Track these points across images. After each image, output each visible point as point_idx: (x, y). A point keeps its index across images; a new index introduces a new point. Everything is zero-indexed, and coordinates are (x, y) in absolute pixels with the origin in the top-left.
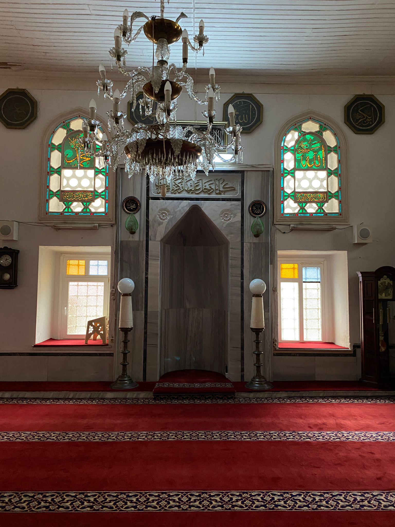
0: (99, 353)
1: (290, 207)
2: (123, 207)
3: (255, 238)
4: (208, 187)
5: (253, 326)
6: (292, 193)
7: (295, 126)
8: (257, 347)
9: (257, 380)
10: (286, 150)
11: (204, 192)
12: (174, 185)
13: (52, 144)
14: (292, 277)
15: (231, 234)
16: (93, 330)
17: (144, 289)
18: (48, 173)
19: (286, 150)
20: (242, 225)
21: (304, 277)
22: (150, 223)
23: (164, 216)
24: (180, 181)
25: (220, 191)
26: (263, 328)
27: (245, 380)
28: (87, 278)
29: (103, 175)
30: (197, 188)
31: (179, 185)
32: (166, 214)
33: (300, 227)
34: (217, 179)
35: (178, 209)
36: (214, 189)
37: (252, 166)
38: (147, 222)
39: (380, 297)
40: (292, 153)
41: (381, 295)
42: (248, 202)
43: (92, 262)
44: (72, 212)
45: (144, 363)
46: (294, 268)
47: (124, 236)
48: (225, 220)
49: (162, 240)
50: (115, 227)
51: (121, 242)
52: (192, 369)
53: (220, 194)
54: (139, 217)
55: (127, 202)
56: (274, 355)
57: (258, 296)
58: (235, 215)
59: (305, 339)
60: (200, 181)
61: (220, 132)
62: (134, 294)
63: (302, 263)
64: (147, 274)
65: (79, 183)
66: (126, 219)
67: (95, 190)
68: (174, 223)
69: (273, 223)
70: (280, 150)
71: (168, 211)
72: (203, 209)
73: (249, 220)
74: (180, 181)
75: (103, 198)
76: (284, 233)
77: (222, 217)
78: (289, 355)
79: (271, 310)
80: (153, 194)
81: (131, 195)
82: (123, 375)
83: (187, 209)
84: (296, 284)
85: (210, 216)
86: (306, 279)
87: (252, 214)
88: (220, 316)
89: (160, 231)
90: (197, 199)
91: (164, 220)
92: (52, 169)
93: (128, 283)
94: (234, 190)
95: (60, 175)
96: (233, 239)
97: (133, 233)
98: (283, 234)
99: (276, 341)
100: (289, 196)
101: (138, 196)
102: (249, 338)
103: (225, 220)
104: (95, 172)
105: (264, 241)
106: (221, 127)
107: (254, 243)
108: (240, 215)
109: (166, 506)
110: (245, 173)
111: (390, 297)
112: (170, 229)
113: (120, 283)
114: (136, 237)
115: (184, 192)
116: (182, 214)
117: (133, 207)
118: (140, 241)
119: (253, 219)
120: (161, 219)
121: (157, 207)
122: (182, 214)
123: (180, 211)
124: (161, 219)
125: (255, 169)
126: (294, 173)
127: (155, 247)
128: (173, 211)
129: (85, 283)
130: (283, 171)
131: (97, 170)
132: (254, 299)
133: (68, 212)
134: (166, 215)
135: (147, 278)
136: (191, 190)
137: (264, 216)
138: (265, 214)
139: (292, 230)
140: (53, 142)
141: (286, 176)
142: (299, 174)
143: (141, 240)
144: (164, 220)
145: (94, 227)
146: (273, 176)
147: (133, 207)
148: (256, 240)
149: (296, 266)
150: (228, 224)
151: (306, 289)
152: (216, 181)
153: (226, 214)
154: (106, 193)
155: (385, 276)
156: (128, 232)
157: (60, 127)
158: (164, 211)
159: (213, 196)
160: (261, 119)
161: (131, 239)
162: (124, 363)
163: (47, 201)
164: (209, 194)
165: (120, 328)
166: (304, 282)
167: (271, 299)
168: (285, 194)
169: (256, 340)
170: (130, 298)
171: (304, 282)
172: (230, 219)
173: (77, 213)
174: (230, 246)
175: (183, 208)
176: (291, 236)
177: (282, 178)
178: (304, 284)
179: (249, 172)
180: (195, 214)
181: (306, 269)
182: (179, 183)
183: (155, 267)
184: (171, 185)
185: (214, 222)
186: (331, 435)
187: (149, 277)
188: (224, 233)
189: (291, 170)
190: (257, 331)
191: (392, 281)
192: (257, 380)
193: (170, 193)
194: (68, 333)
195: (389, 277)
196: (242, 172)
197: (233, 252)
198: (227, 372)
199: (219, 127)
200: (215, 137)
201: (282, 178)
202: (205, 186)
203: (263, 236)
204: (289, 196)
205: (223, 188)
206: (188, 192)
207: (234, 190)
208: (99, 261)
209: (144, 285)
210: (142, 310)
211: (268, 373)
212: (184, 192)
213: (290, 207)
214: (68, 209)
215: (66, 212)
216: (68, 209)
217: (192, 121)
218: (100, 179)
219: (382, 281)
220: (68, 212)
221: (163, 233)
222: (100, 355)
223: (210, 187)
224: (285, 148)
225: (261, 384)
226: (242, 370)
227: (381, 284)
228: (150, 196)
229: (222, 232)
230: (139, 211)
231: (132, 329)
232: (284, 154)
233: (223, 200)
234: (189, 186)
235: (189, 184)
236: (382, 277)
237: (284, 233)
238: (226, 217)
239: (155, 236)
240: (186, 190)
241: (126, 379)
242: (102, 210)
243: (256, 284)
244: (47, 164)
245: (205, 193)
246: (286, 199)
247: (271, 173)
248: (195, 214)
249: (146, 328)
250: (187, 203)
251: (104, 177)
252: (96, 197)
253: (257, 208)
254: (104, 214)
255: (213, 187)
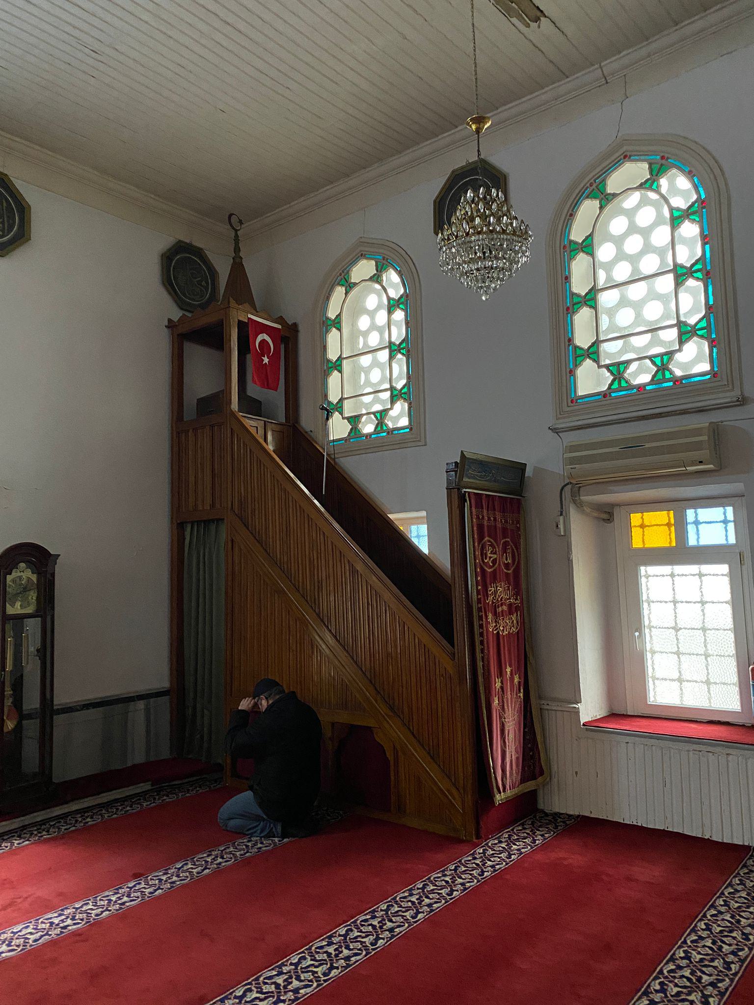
13: (571, 242)
18: (568, 309)
28: (681, 553)
39: (10, 610)
41: (13, 605)
43: (690, 514)
44: (630, 387)
65: (638, 315)
75: (702, 337)
92: (576, 300)
95: (595, 308)
111: (30, 610)
133: (620, 389)
140: (572, 238)
155: (22, 565)
157: (587, 197)
163: (572, 372)
173: (641, 388)
181: (668, 525)
186: (23, 933)
191: (35, 575)
195: (29, 563)
208: (699, 511)
214: (620, 383)
215: (615, 391)
216: (620, 383)
218: (692, 292)
219: (15, 574)
220: (620, 389)
227: (13, 581)
236: (16, 566)
242: (705, 367)
244: (564, 291)
251: (700, 284)
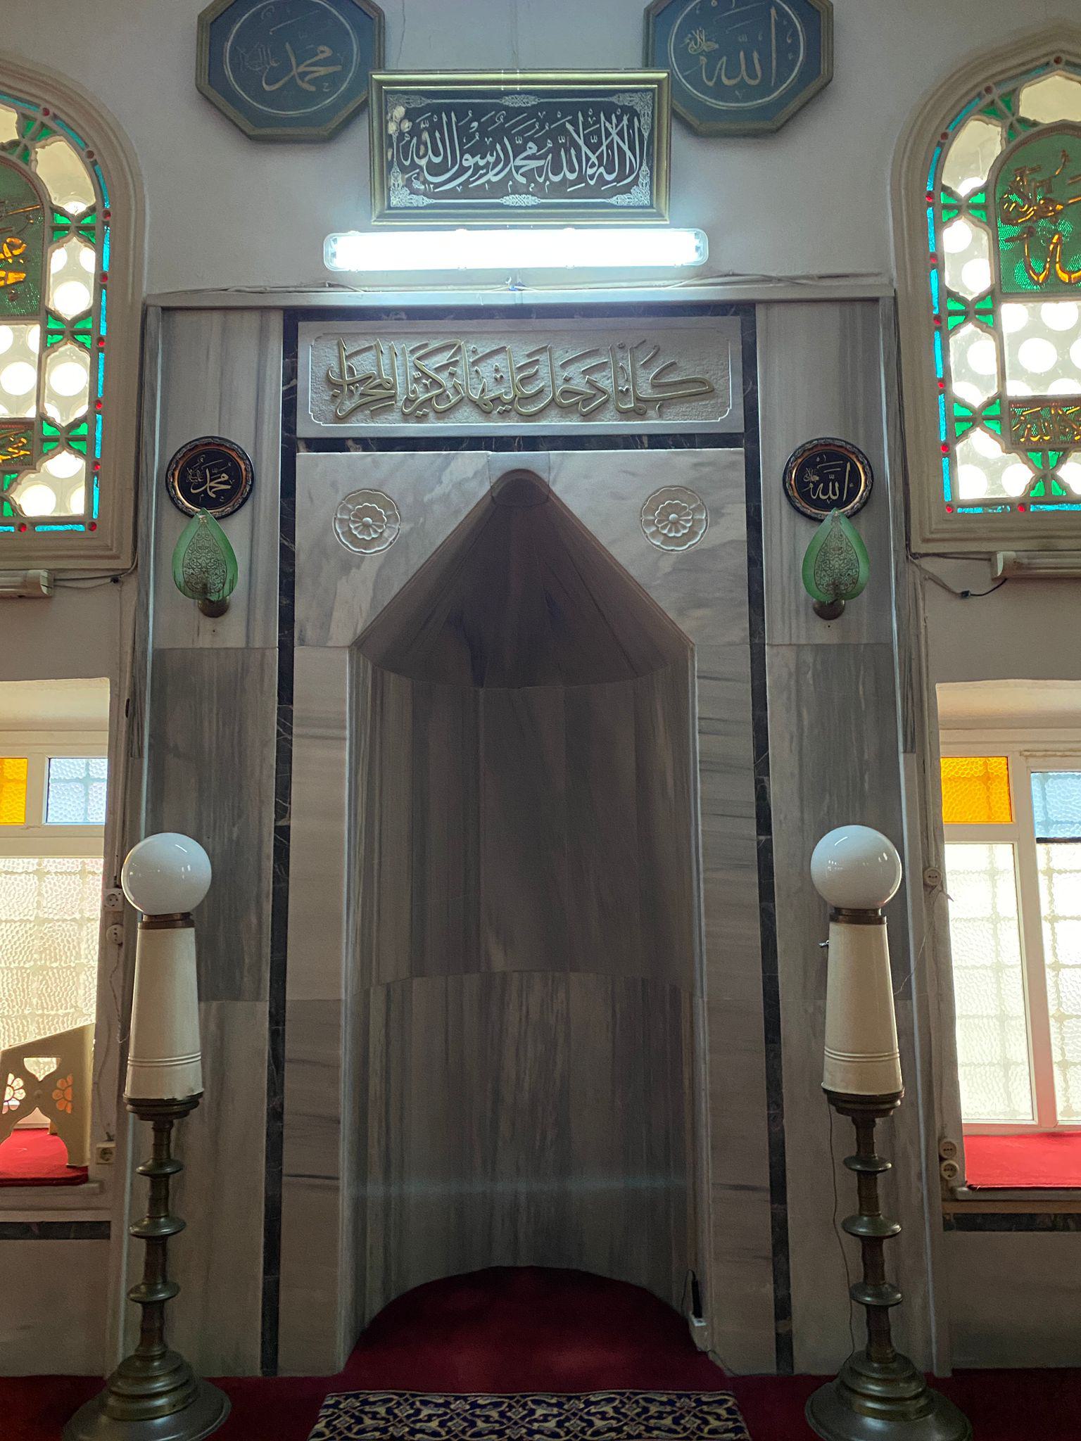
0: (40, 1225)
1: (985, 472)
2: (169, 487)
3: (820, 624)
4: (579, 384)
5: (837, 1080)
6: (990, 403)
7: (988, 98)
8: (868, 1202)
9: (875, 1389)
10: (948, 207)
11: (561, 407)
12: (416, 380)
14: (982, 818)
15: (700, 604)
16: (21, 1094)
17: (268, 884)
19: (948, 207)
20: (754, 561)
21: (1038, 817)
22: (301, 560)
23: (366, 526)
24: (442, 359)
25: (638, 399)
26: (896, 1096)
27: (802, 1365)
29: (82, 345)
30: (530, 390)
31: (442, 377)
32: (376, 515)
33: (1046, 562)
34: (622, 347)
35: (438, 491)
36: (610, 390)
37: (792, 281)
38: (288, 555)
40: (976, 222)
42: (777, 454)
45: (267, 1272)
46: (987, 778)
47: (171, 623)
48: (667, 540)
49: (359, 645)
50: (130, 586)
51: (159, 654)
52: (521, 1264)
53: (639, 413)
54: (246, 536)
55: (191, 463)
56: (948, 1226)
57: (861, 916)
58: (717, 513)
59: (1063, 1119)
60: (543, 358)
61: (631, 121)
62: (212, 919)
63: (1028, 754)
64: (282, 811)
66: (183, 538)
67: (42, 417)
68: (417, 559)
69: (908, 546)
70: (924, 202)
71: (388, 505)
72: (557, 489)
73: (788, 537)
74: (442, 359)
76: (965, 594)
77: (651, 523)
78: (1026, 1223)
79: (921, 989)
80: (311, 423)
81: (207, 428)
82: (144, 1357)
83: (482, 490)
84: (1004, 854)
85: (592, 523)
86: (1047, 824)
87: (801, 504)
88: (655, 1018)
89: (350, 598)
90: (531, 443)
91: (368, 544)
93: (182, 859)
94: (710, 393)
96: (710, 633)
97: (216, 610)
98: (958, 604)
99: (952, 1149)
100: (976, 419)
101: (239, 435)
102: (816, 1143)
103: (667, 540)
104: (46, 333)
105: (865, 641)
106: (636, 97)
107: (819, 648)
108: (740, 511)
109: (464, 1432)
110: (760, 313)
112: (396, 590)
113: (132, 860)
114: (231, 632)
115: (466, 411)
116: (457, 512)
117: (219, 484)
118: (248, 648)
119: (805, 534)
120: (354, 540)
121: (334, 485)
122: (457, 512)
123: (445, 498)
124: (354, 540)
125: (808, 300)
126: (993, 312)
127: (328, 679)
128: (410, 500)
129: (31, 863)
130: (942, 303)
131: (52, 325)
132: (838, 937)
134: (381, 521)
135: (283, 834)
136: (497, 400)
137: (863, 514)
138: (865, 503)
139: (1002, 581)
141: (957, 328)
142: (1013, 315)
143: (258, 643)
144: (368, 544)
145: (24, 585)
146: (897, 325)
147: (219, 484)
148: (824, 633)
149: (997, 765)
150: (686, 558)
151: (1050, 872)
152: (620, 354)
153: (678, 509)
154: (92, 429)
156: (191, 606)
158: (367, 504)
159: (608, 424)
160: (824, 67)
161: (205, 642)
162: (152, 1290)
164: (586, 416)
165: (132, 1101)
166: (1040, 840)
167: (909, 924)
168: (959, 411)
169: (857, 1159)
170: (186, 940)
171: (1040, 840)
172: (692, 533)
174: (697, 665)
175: (459, 485)
176: (997, 615)
177: (937, 335)
178: (1040, 848)
179: (776, 310)
180: (520, 508)
181: (1046, 779)
182: (438, 370)
183: (328, 778)
184: (399, 380)
185: (614, 551)
187: (295, 824)
188: (665, 600)
189: (981, 298)
190: (864, 1111)
192: (875, 1389)
193: (396, 415)
194: (937, 686)
196: (744, 310)
197: (713, 697)
198: (698, 1314)
199: (625, 100)
200: (610, 147)
201: (937, 335)
202: (567, 380)
203: (858, 611)
204: (976, 419)
205: (654, 386)
206: (484, 408)
207: (710, 393)
209: (269, 865)
210: (257, 997)
211: (923, 1333)
212: (466, 411)
213: (985, 472)
217: (498, 71)
221: (366, 606)
222: (47, 1231)
223: (591, 383)
224: (944, 199)
225: (904, 1416)
226: (783, 1309)
228: (303, 431)
229: (653, 595)
230: (249, 503)
231: (193, 1101)
232: (940, 225)
233: (657, 441)
234: (488, 379)
235: (486, 370)
237: (965, 594)
238: (675, 523)
239: (325, 622)
240: (474, 403)
241: (159, 1386)
243: (843, 849)
245: (566, 410)
246: (965, 434)
247: (883, 309)
248: (520, 508)
249: (276, 1086)
250: (483, 461)
252: (48, 446)
253: (826, 475)
254: (81, 528)
255: (605, 382)
